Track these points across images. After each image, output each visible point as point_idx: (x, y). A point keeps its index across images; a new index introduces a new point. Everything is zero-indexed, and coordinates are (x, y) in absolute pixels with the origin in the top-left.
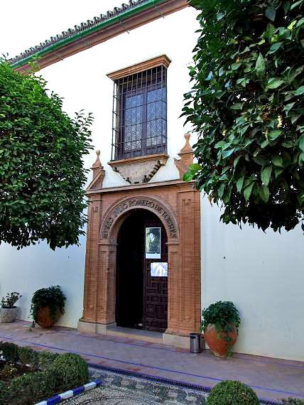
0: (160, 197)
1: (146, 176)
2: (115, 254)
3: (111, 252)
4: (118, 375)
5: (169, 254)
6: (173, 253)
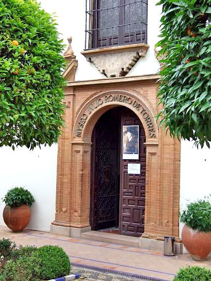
0: (139, 93)
1: (123, 69)
2: (89, 155)
3: (85, 152)
4: (95, 271)
5: (147, 154)
6: (153, 154)
